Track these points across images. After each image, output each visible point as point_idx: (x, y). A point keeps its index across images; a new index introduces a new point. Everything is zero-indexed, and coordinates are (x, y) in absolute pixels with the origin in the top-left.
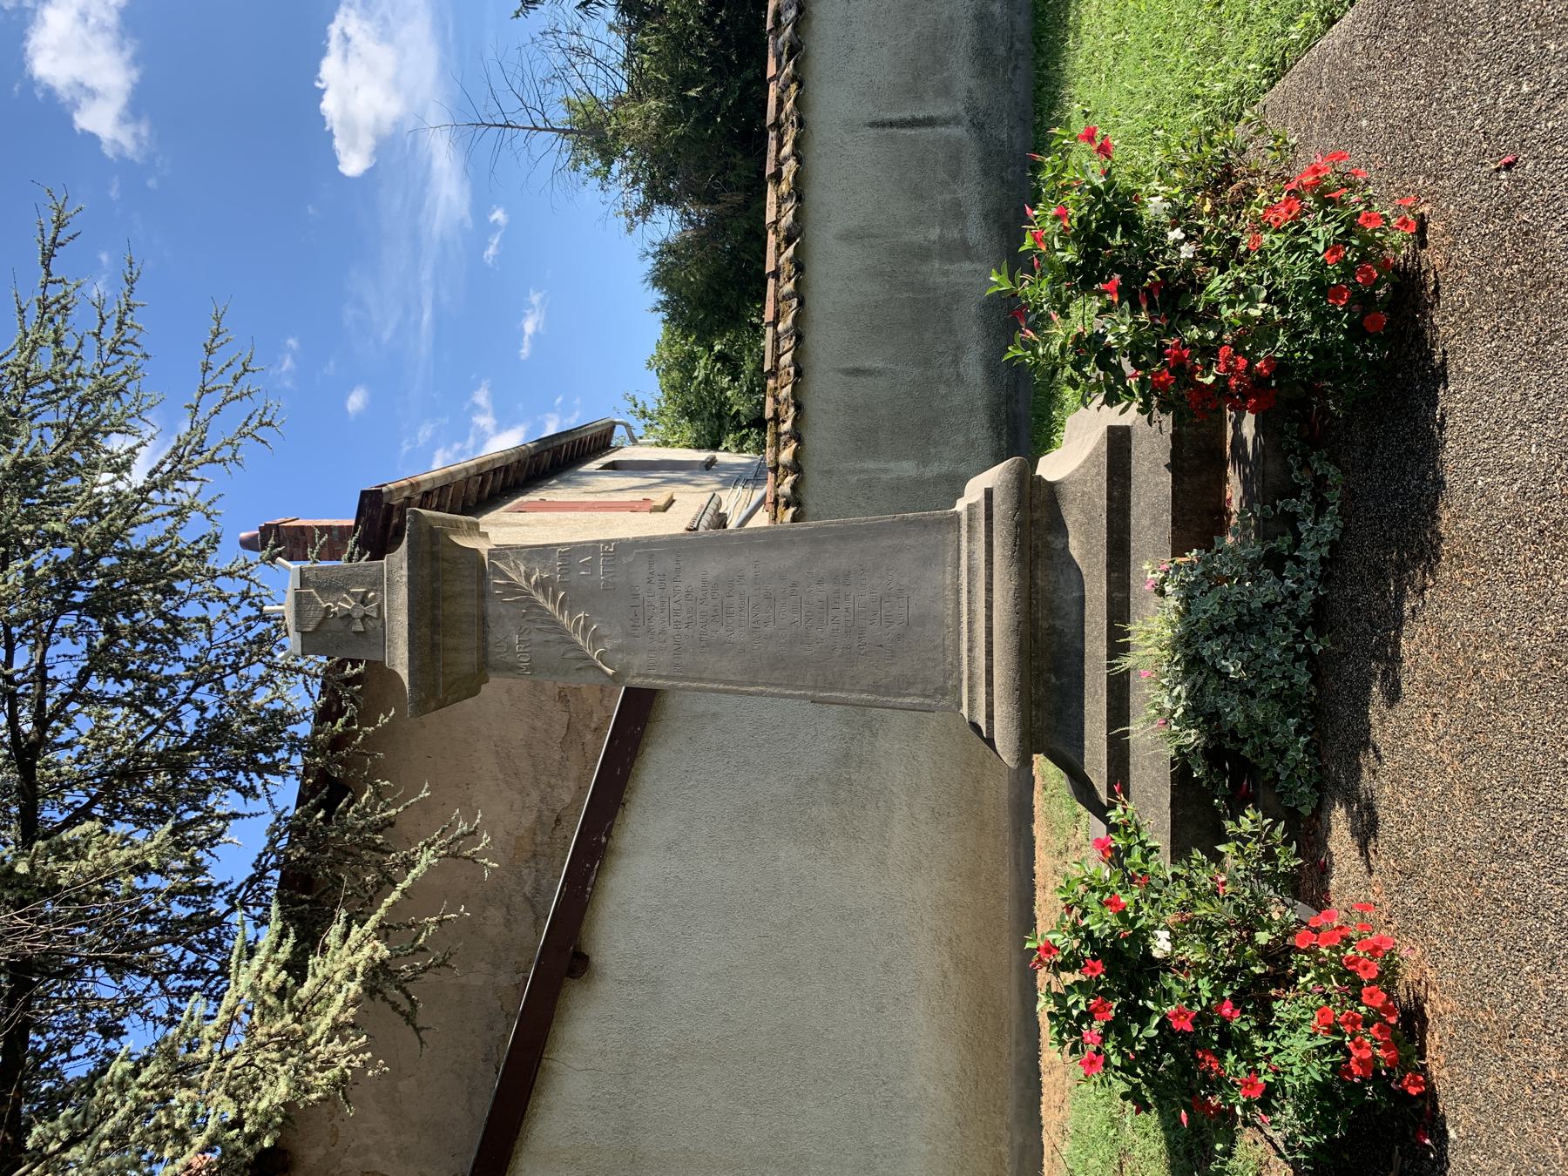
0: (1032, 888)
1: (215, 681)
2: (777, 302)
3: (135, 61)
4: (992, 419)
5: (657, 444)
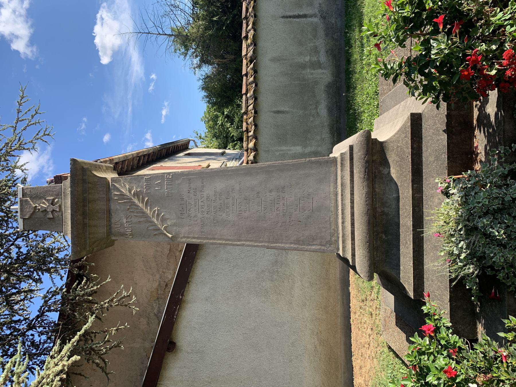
0: (349, 313)
1: (25, 236)
2: (247, 85)
3: (32, 26)
4: (331, 130)
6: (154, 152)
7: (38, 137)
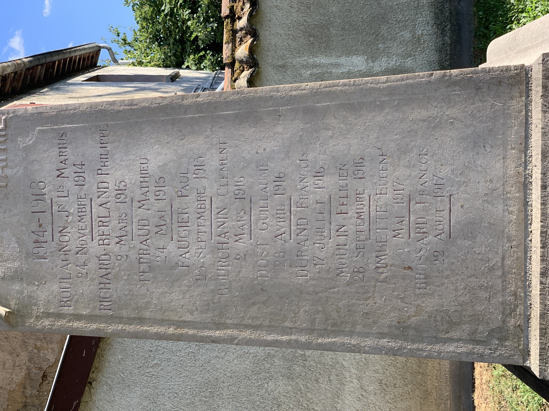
6: (16, 73)
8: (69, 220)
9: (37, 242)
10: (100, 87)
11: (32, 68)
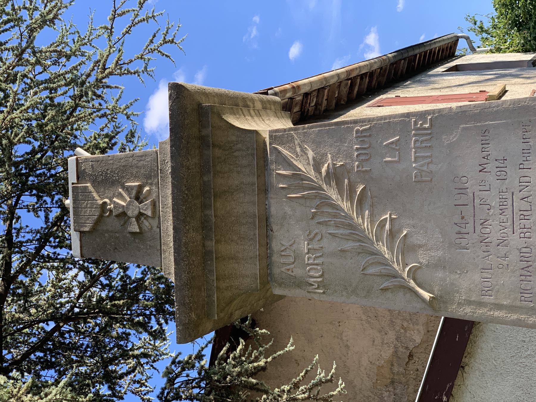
5: (491, 51)
6: (381, 68)
7: (152, 47)
8: (490, 213)
9: (459, 233)
10: (460, 77)
11: (396, 63)
